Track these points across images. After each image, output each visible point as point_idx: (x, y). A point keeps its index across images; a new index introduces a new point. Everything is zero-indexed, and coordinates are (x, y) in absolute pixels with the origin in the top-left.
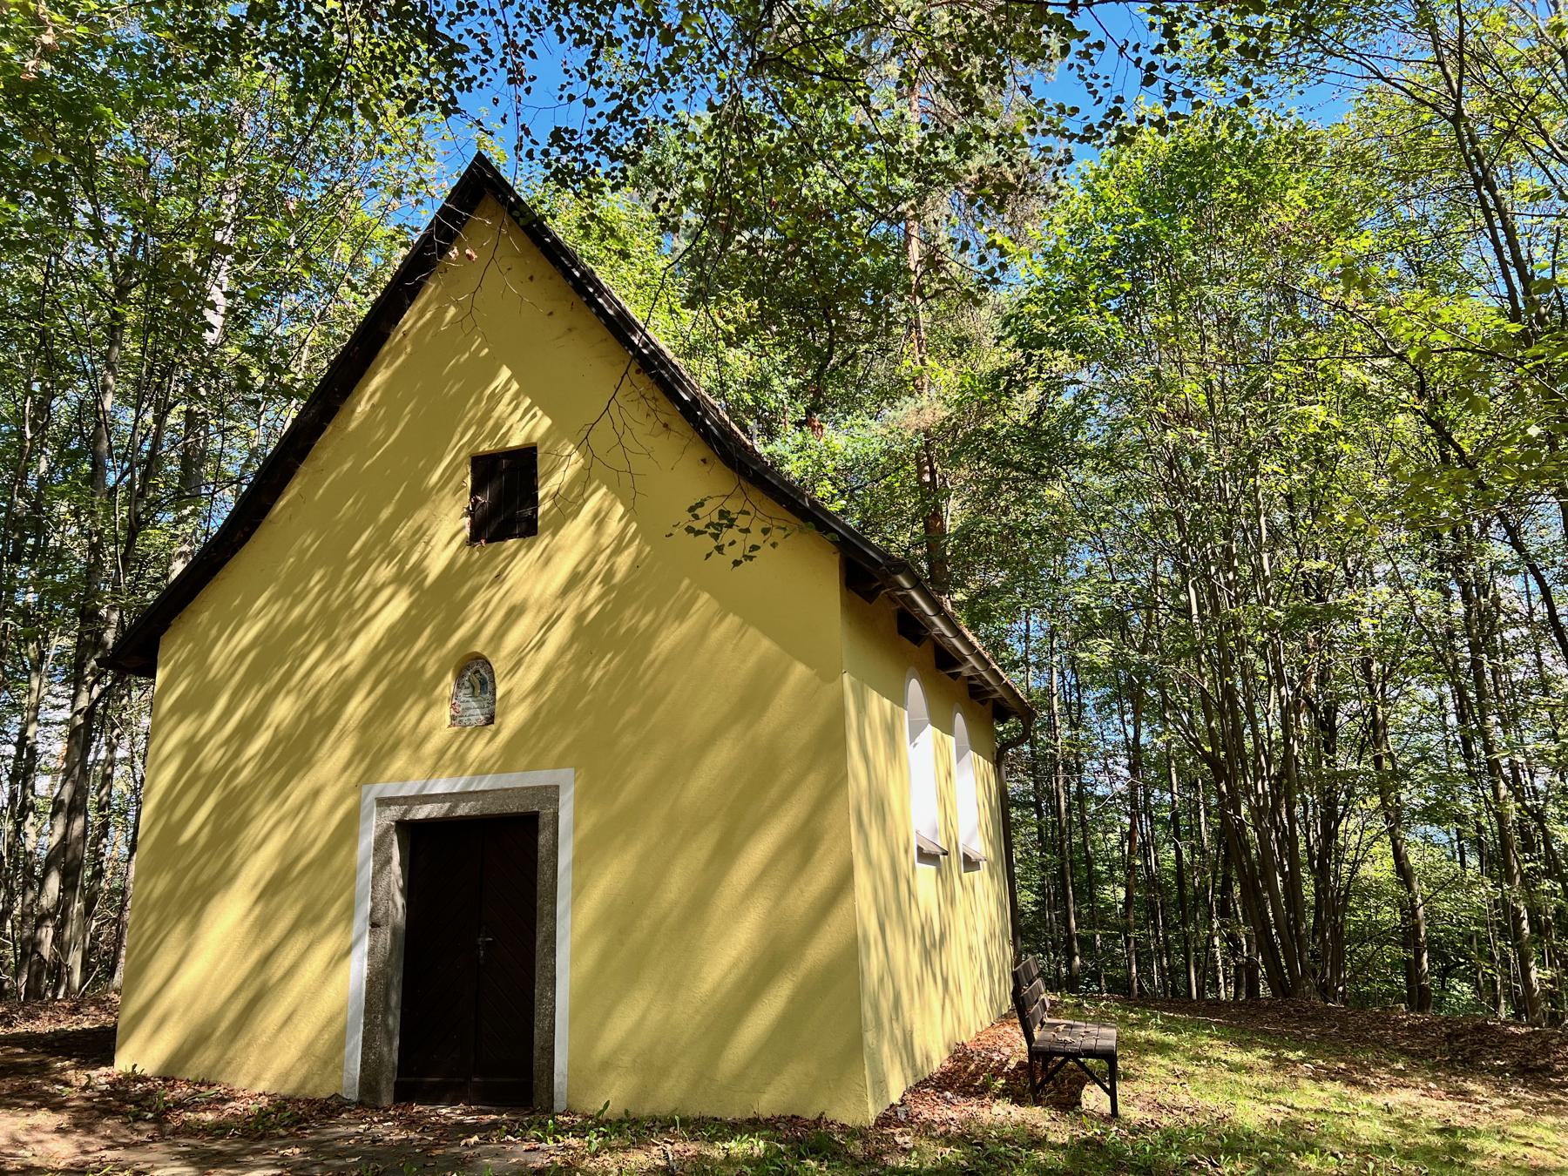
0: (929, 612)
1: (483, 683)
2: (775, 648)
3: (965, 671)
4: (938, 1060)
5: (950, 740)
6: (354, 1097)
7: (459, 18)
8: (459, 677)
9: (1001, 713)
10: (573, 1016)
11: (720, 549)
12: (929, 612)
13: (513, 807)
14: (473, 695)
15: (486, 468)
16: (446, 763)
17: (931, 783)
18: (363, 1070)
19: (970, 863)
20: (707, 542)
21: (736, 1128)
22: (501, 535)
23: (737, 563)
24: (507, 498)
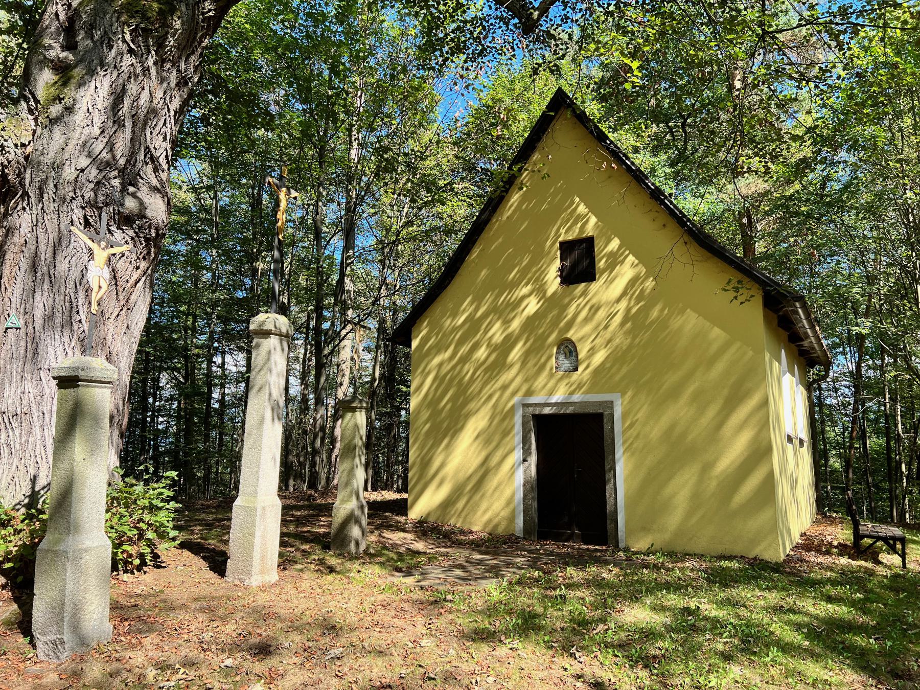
0: (803, 317)
1: (570, 352)
2: (724, 334)
3: (806, 343)
4: (797, 539)
5: (794, 379)
6: (522, 536)
7: (561, 26)
8: (558, 348)
9: (811, 363)
10: (627, 507)
11: (736, 298)
12: (803, 317)
13: (590, 410)
14: (566, 357)
15: (567, 248)
16: (557, 392)
17: (789, 401)
18: (524, 524)
19: (801, 442)
20: (732, 294)
21: (731, 558)
22: (578, 281)
23: (742, 303)
24: (580, 263)
